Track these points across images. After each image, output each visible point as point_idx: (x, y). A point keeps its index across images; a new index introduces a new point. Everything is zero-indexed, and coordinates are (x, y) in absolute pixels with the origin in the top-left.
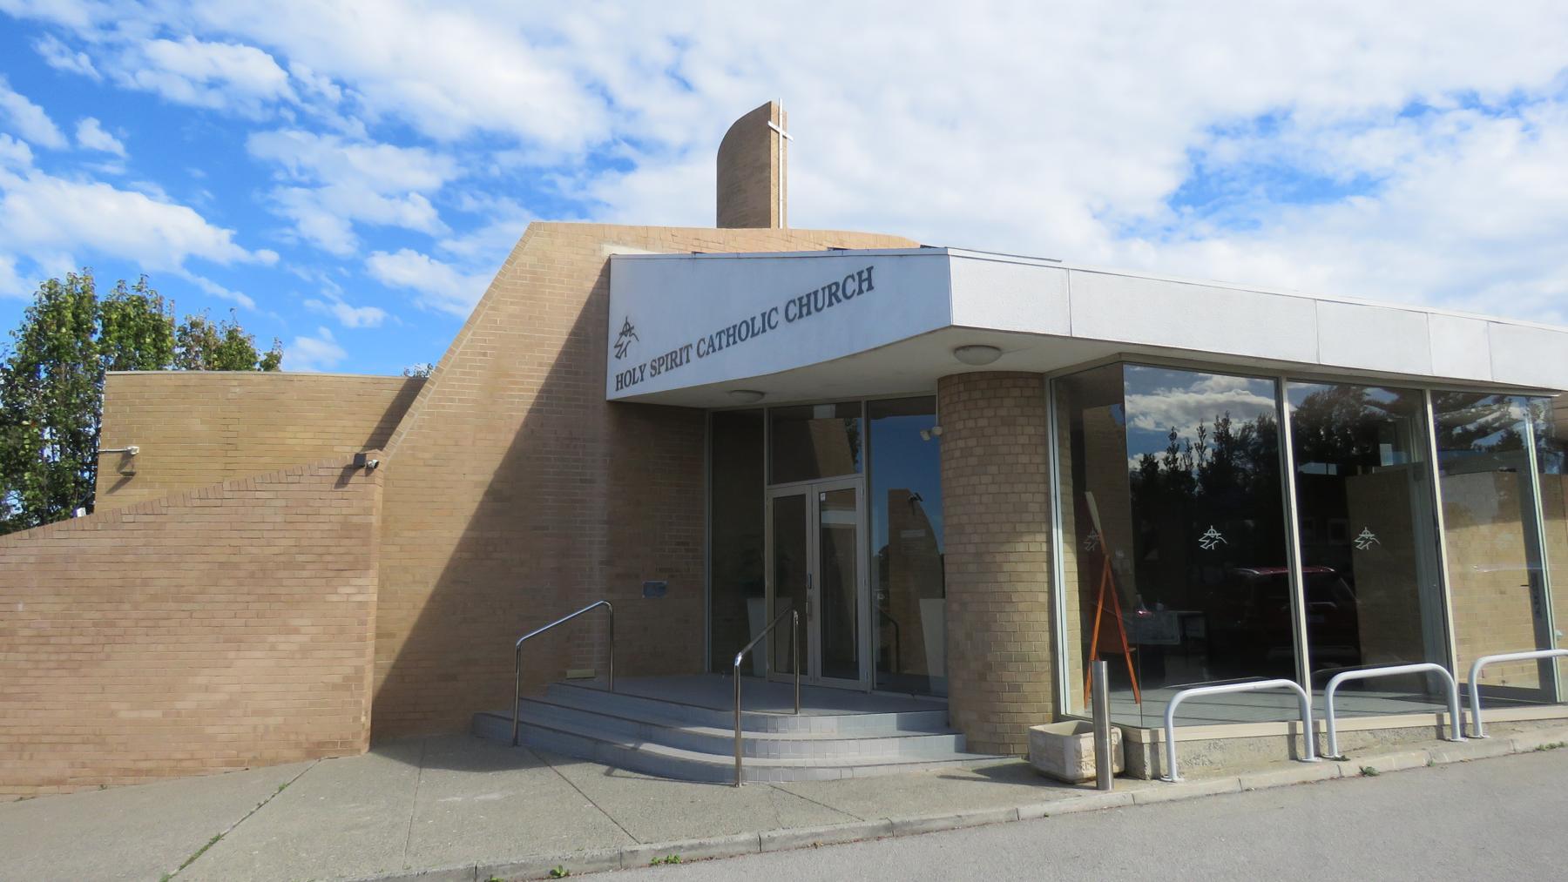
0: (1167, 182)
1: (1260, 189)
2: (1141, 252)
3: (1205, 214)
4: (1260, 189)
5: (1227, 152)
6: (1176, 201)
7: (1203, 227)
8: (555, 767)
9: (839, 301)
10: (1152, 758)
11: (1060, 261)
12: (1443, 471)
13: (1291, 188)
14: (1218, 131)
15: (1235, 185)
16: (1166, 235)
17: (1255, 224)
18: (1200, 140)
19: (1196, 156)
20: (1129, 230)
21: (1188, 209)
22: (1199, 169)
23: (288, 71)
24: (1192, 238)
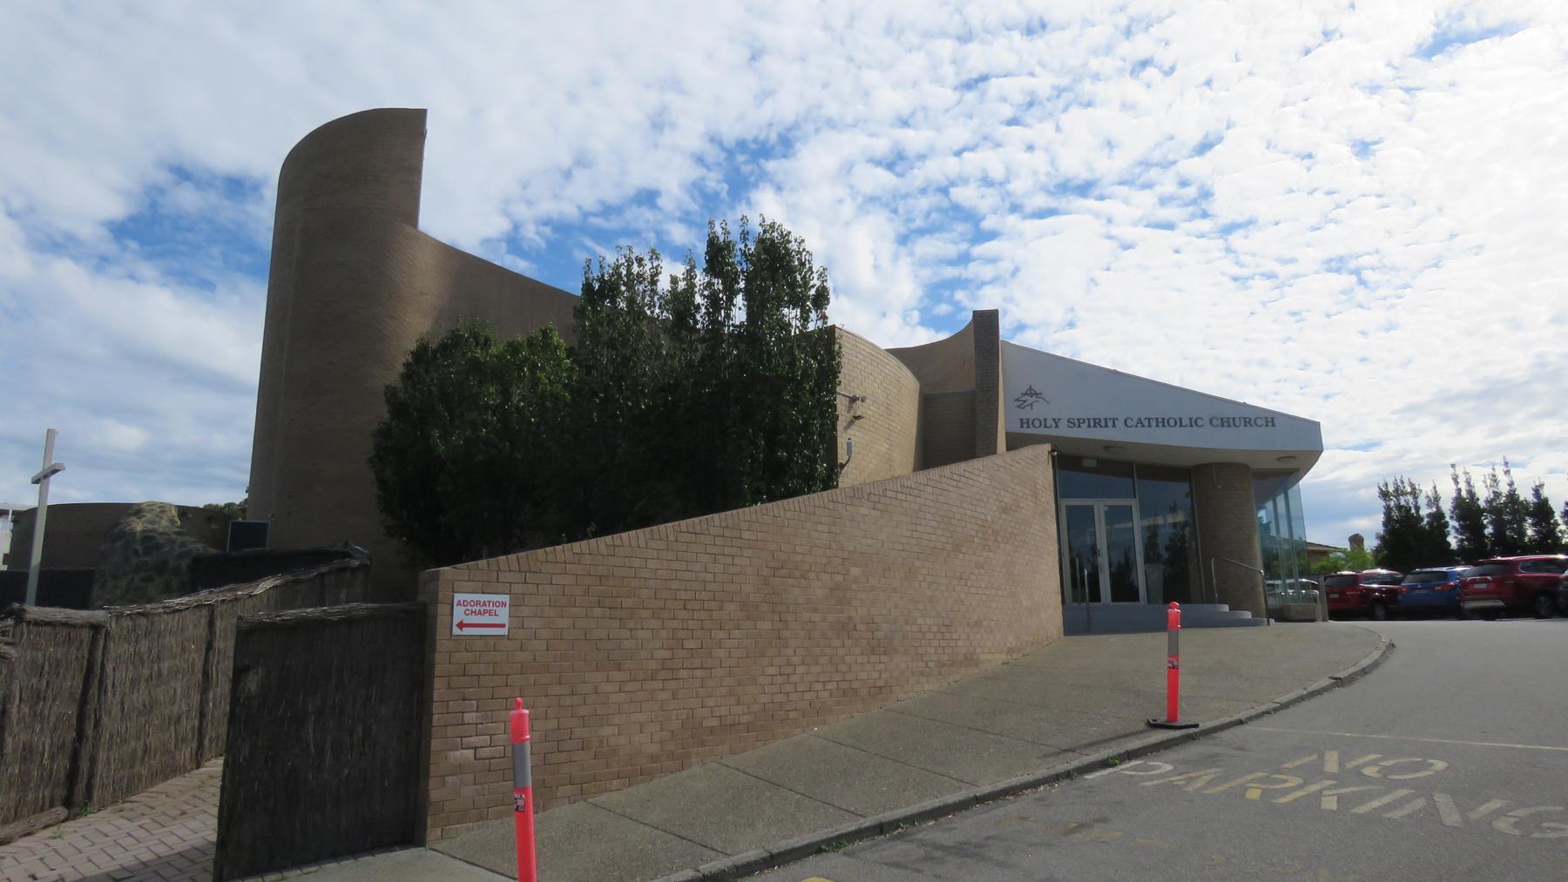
0: (116, 209)
1: (216, 250)
2: (67, 274)
3: (149, 257)
4: (216, 250)
5: (188, 199)
6: (121, 230)
7: (147, 270)
8: (98, 872)
9: (1252, 426)
10: (1076, 574)
11: (1377, 444)
12: (464, 558)
13: (247, 259)
14: (182, 174)
15: (190, 237)
16: (101, 263)
17: (206, 285)
18: (162, 177)
19: (154, 193)
20: (54, 244)
21: (133, 245)
22: (154, 206)
23: (978, 259)
24: (132, 277)
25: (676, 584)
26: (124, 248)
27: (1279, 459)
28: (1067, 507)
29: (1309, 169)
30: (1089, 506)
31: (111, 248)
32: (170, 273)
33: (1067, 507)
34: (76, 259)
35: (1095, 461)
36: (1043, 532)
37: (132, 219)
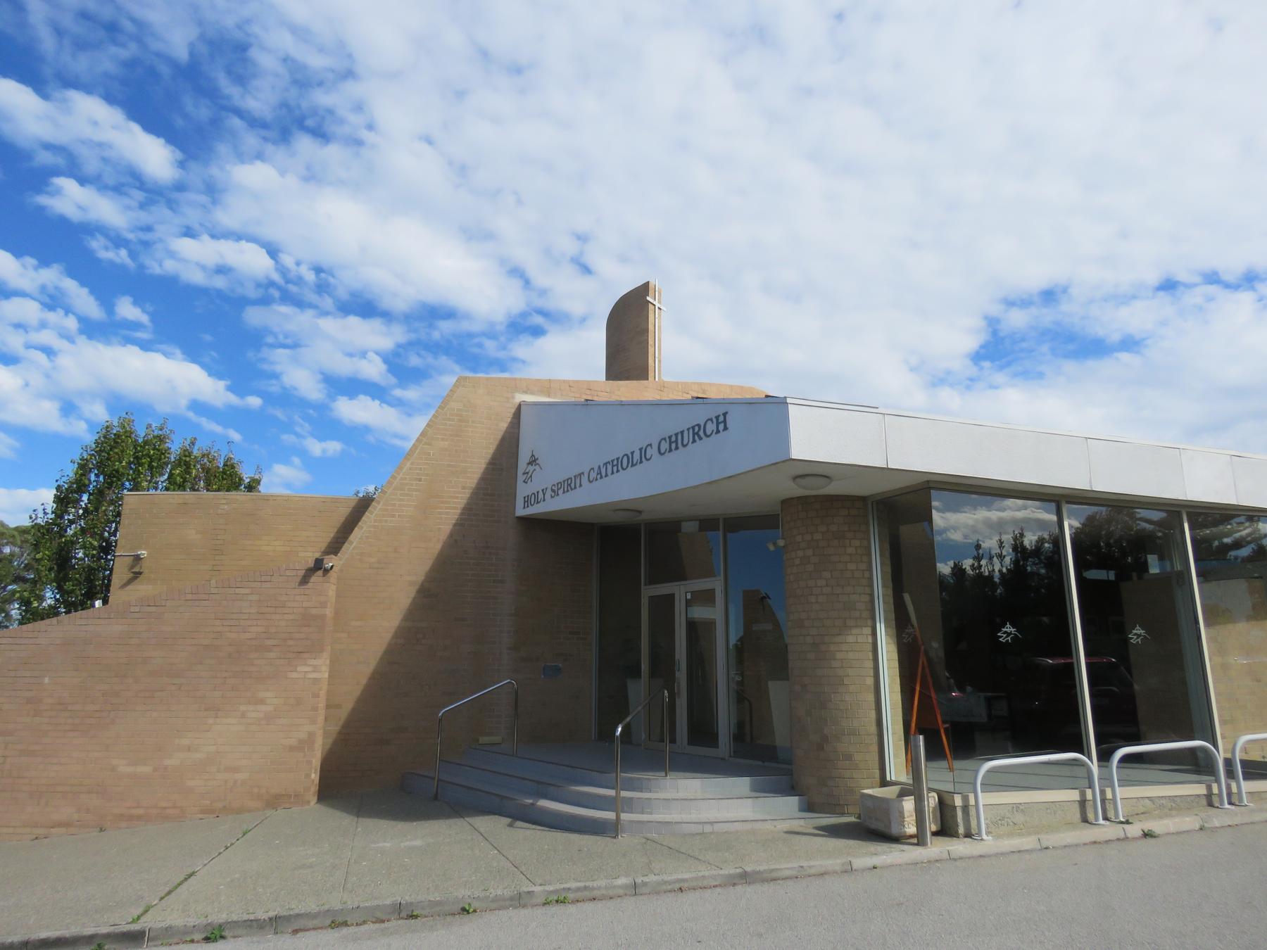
0: (971, 343)
1: (1045, 348)
2: (950, 398)
3: (1002, 368)
5: (1017, 319)
6: (977, 357)
7: (1000, 378)
13: (1071, 347)
15: (1024, 345)
16: (970, 383)
17: (1041, 375)
20: (939, 380)
21: (987, 364)
22: (995, 333)
25: (291, 643)
26: (981, 369)
27: (796, 478)
28: (690, 743)
29: (520, 202)
30: (718, 744)
31: (973, 371)
32: (1015, 375)
33: (690, 743)
34: (952, 386)
35: (698, 522)
36: (314, 671)
37: (982, 347)
